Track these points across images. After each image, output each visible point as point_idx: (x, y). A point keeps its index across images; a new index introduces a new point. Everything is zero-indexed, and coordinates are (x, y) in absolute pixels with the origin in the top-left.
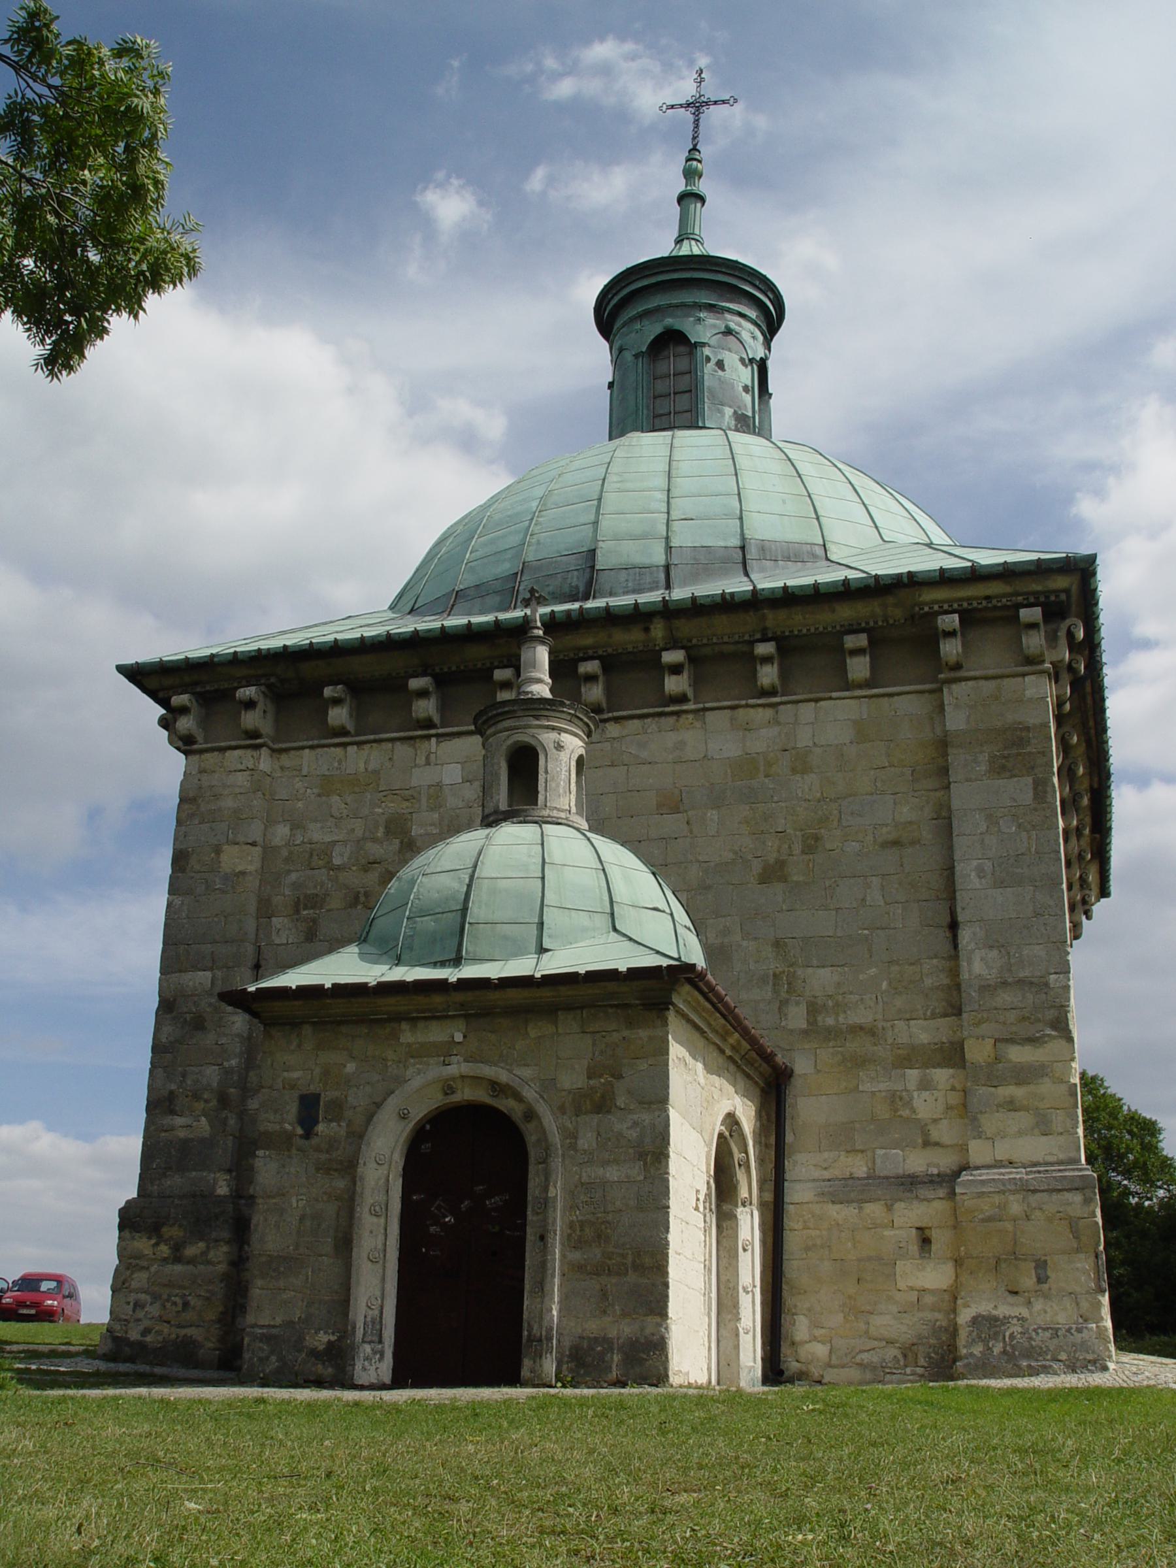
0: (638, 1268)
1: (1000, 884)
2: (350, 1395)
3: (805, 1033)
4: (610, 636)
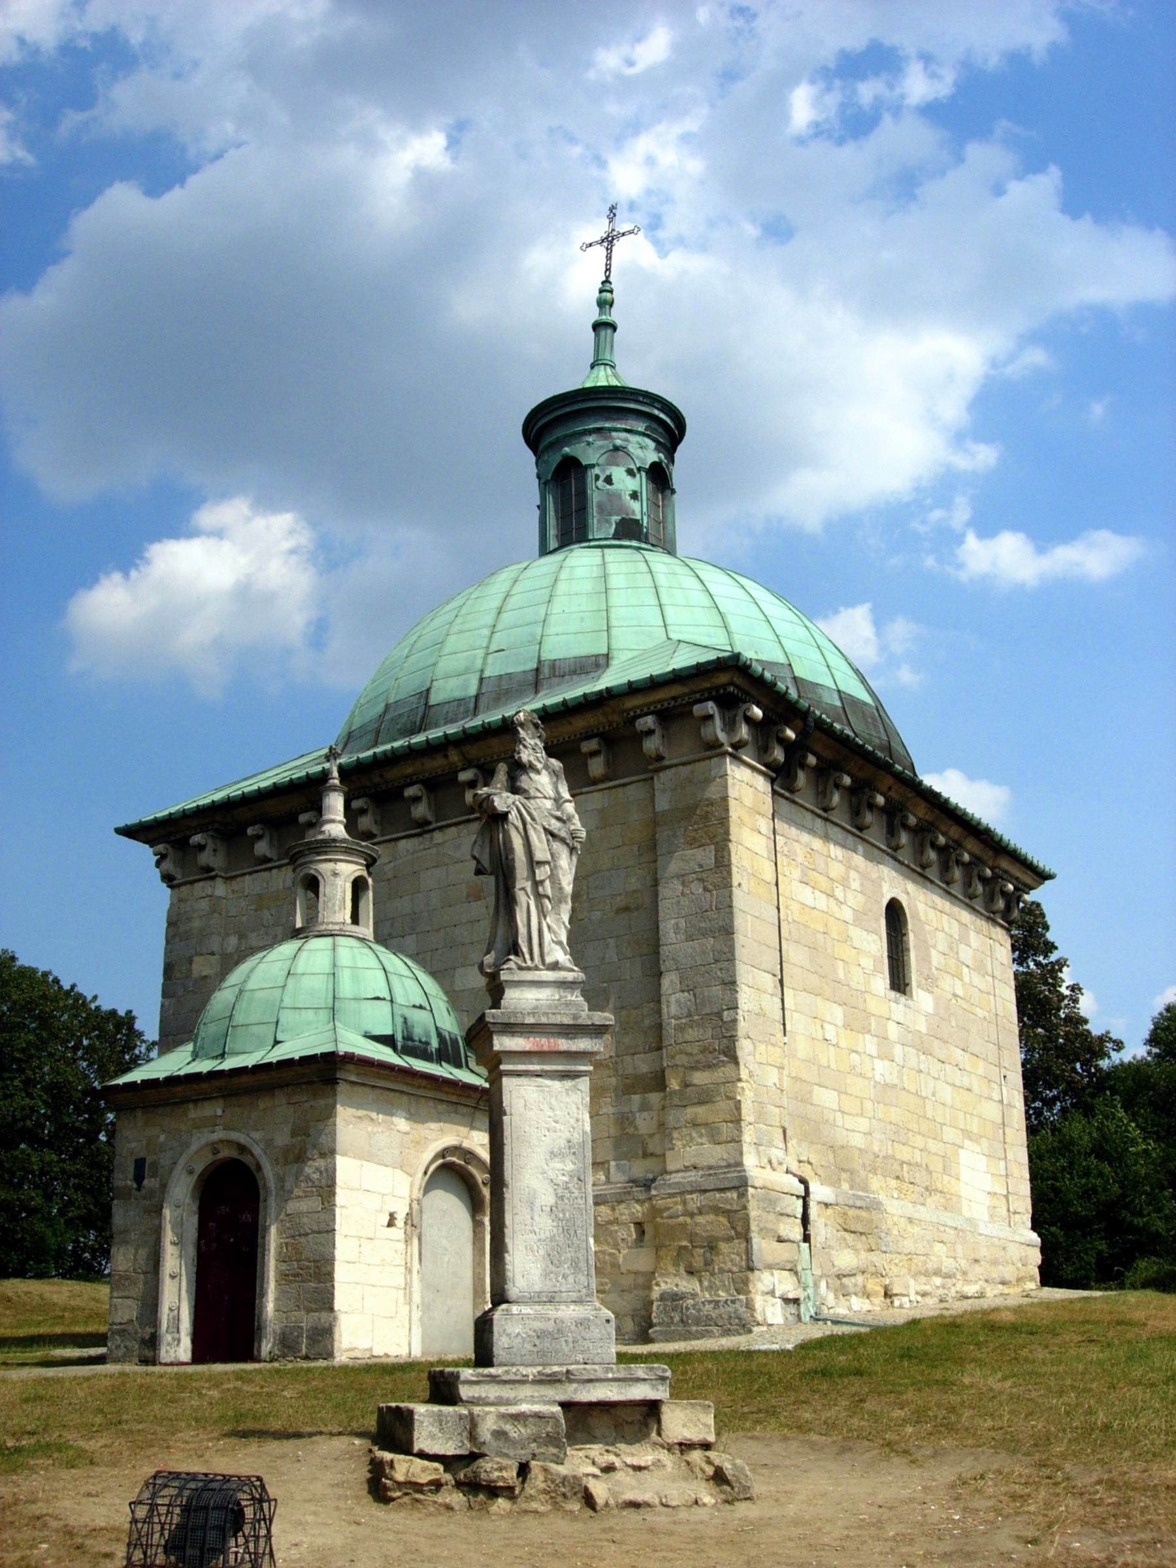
1: (690, 938)
2: (257, 1366)
4: (423, 764)
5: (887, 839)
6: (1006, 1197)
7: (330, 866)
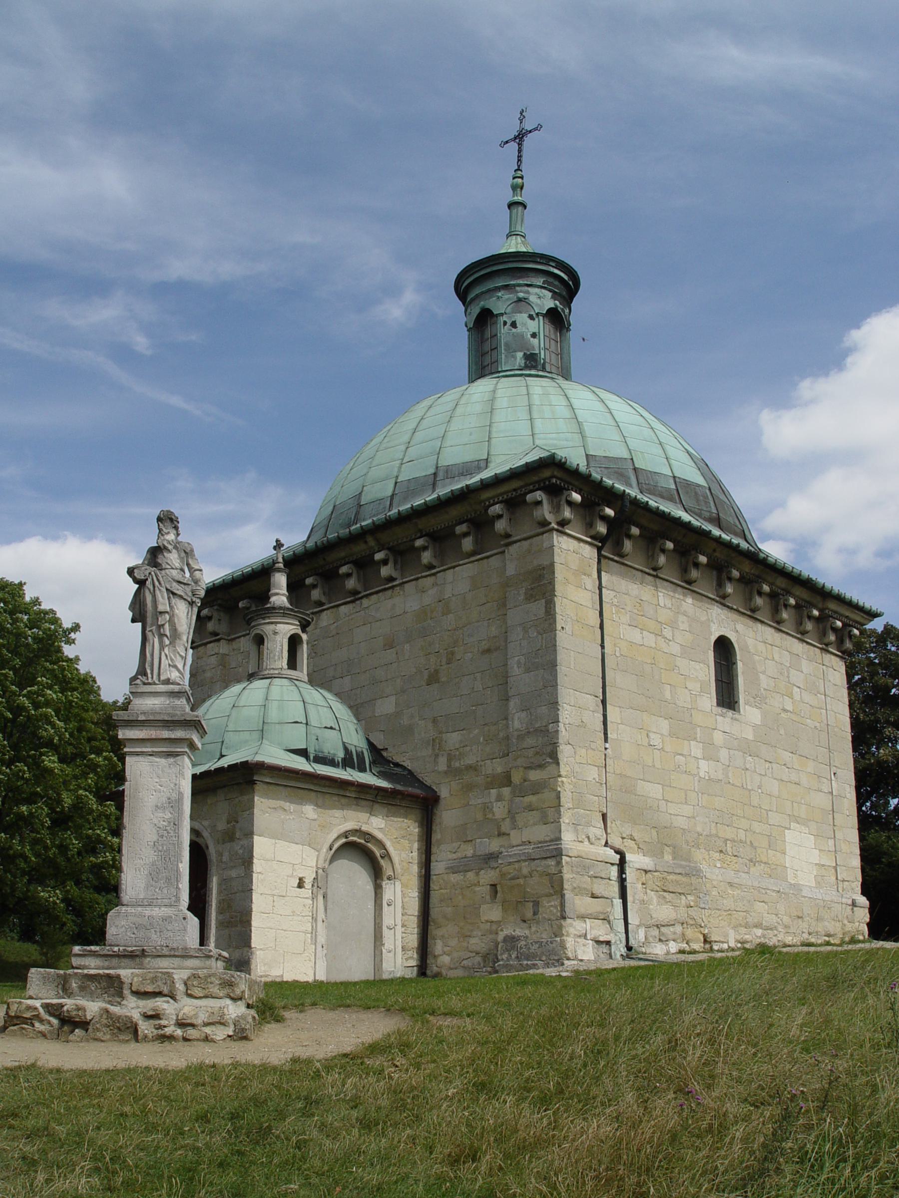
0: (241, 922)
1: (528, 671)
3: (446, 772)
5: (716, 590)
6: (835, 868)
7: (272, 627)
